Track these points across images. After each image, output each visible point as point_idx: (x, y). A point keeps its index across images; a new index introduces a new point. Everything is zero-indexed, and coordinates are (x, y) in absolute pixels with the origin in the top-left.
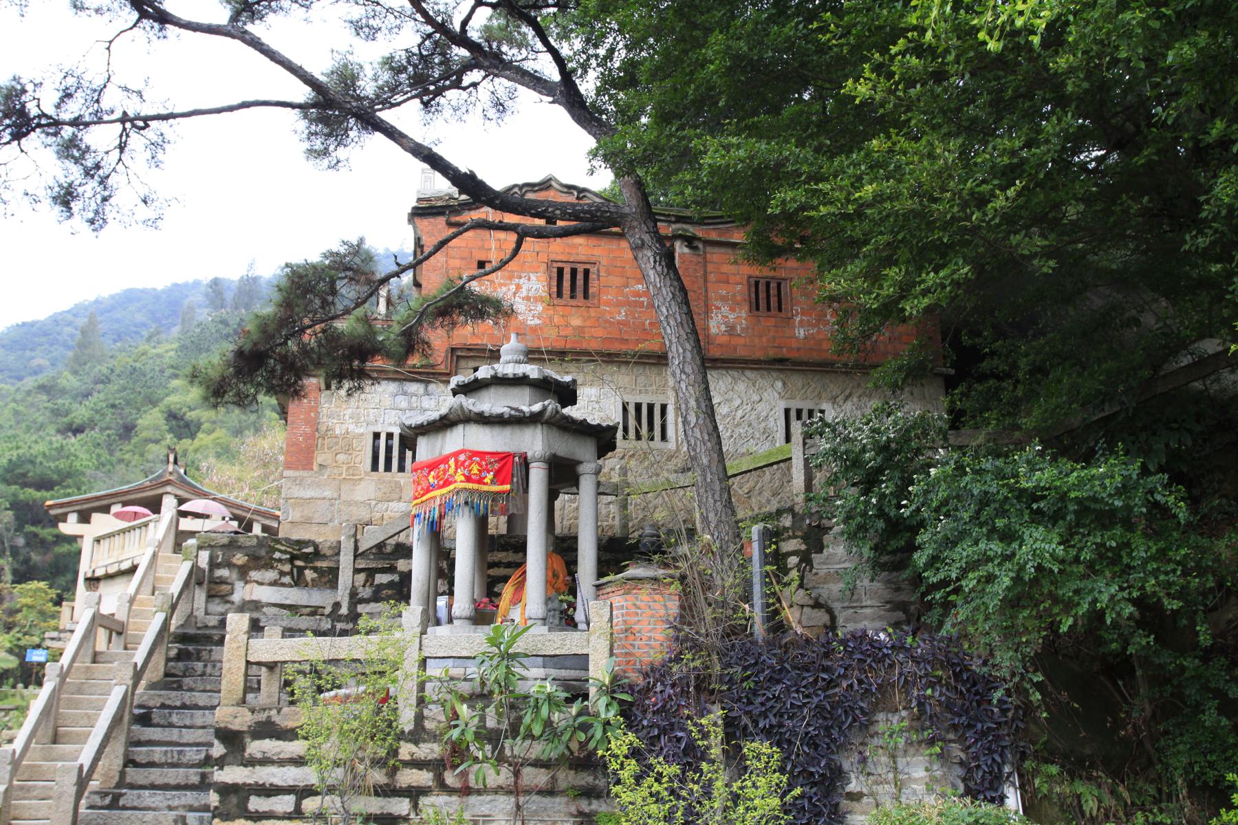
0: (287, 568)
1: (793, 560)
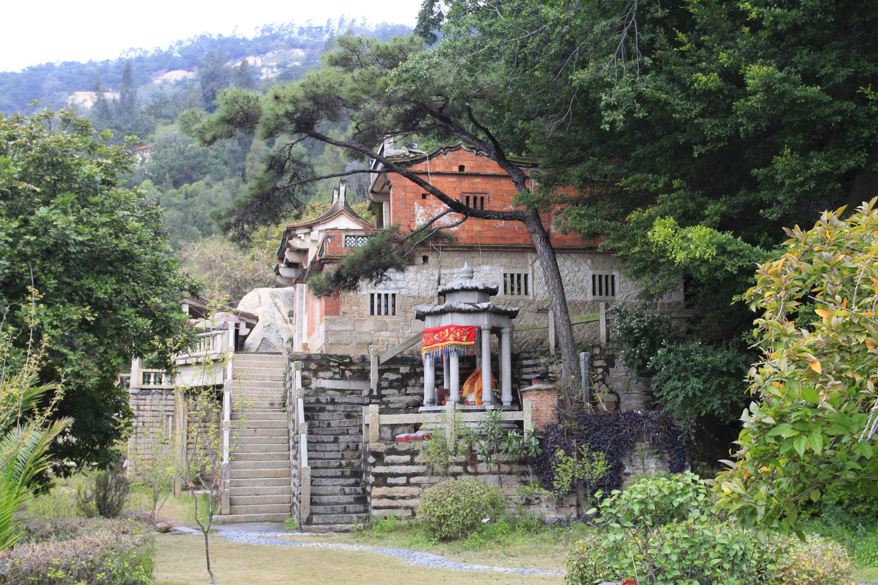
0: (337, 370)
1: (600, 370)
